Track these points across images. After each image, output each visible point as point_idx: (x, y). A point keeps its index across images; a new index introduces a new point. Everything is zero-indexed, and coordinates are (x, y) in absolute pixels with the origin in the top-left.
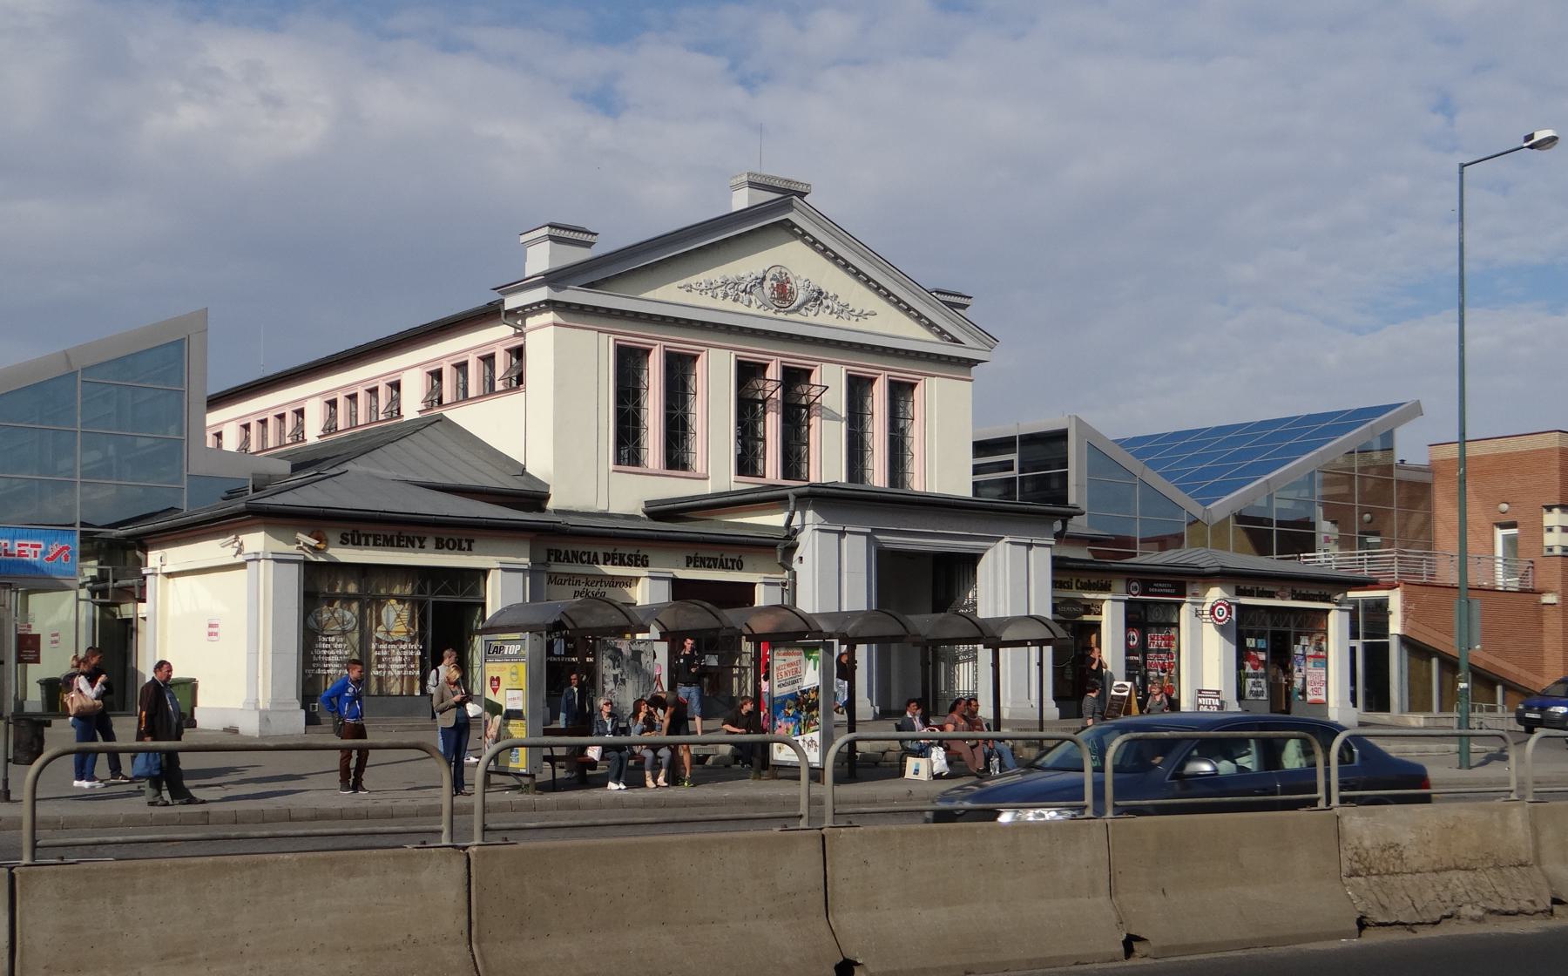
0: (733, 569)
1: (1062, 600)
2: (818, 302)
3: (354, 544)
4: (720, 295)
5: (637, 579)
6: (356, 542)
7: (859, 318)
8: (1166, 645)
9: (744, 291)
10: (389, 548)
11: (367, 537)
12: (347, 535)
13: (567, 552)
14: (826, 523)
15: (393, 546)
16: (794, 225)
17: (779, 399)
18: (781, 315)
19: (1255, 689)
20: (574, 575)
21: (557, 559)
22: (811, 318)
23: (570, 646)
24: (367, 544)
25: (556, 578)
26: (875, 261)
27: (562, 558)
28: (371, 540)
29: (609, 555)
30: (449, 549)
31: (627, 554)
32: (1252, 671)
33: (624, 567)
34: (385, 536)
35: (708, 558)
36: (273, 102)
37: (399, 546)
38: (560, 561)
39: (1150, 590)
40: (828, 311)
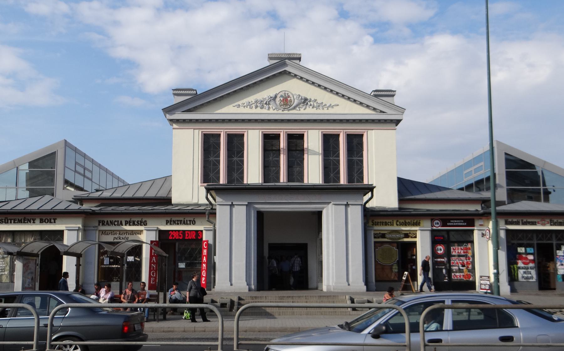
0: (190, 224)
1: (389, 231)
2: (305, 104)
3: (5, 223)
4: (254, 107)
5: (141, 231)
6: (6, 222)
7: (329, 108)
8: (464, 253)
9: (266, 104)
10: (20, 224)
11: (11, 220)
12: (3, 220)
13: (107, 221)
14: (224, 201)
15: (22, 223)
16: (290, 73)
17: (285, 148)
18: (286, 112)
19: (525, 275)
20: (114, 231)
21: (103, 224)
23: (111, 260)
24: (11, 223)
25: (105, 233)
26: (332, 82)
27: (105, 224)
28: (13, 221)
29: (127, 221)
30: (46, 223)
32: (523, 265)
33: (135, 226)
34: (18, 219)
36: (531, 66)
37: (24, 222)
38: (104, 225)
39: (448, 224)
40: (311, 107)
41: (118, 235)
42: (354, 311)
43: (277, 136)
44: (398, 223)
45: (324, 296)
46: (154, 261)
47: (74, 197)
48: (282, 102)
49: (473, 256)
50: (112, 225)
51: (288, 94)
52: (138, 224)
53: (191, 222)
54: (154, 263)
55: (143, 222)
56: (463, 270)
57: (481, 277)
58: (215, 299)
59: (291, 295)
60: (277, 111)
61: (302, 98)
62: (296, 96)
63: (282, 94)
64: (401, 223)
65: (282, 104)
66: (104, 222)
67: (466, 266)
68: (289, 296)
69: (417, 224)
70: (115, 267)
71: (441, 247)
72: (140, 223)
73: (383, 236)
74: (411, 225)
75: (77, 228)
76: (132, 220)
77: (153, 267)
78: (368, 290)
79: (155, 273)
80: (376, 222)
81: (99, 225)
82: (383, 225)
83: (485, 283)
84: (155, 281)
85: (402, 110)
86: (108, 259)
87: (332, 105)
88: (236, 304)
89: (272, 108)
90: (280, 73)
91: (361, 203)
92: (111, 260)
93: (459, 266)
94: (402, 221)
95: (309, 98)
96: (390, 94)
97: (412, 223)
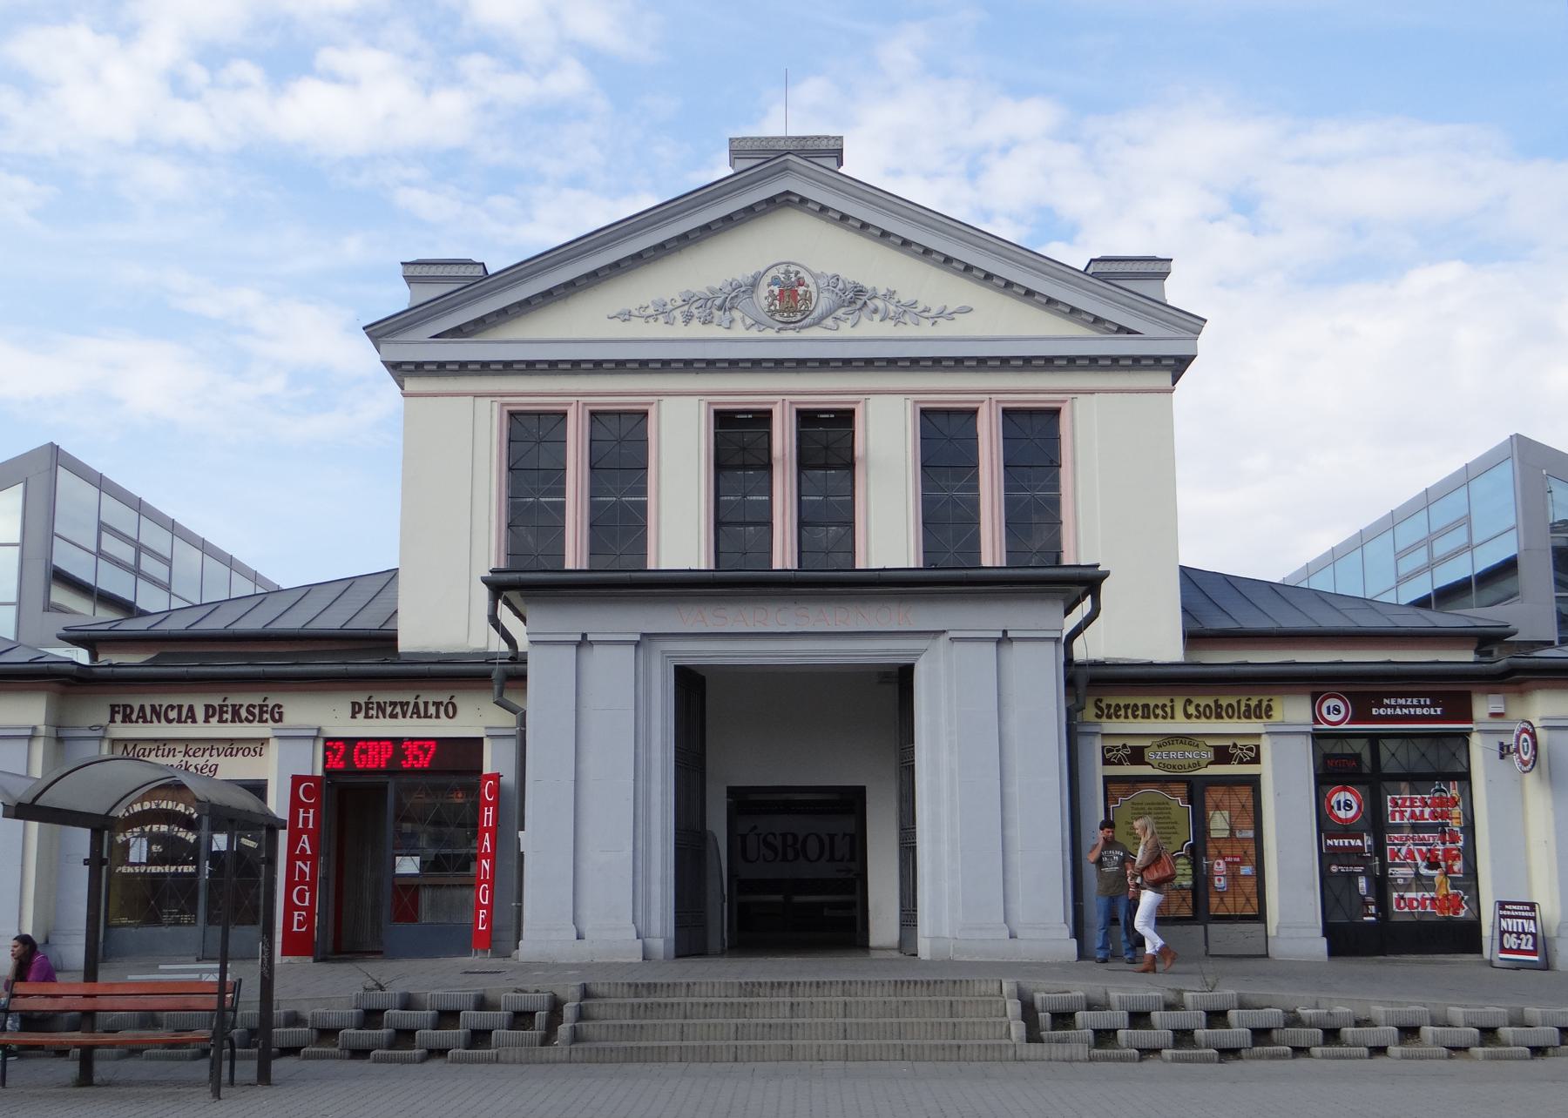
0: (438, 716)
4: (680, 318)
5: (264, 741)
8: (1434, 815)
9: (720, 308)
13: (142, 708)
18: (790, 334)
20: (165, 741)
21: (127, 719)
22: (846, 330)
25: (134, 748)
29: (360, 705)
31: (1132, 704)
35: (391, 703)
38: (131, 721)
39: (1375, 711)
41: (179, 756)
42: (1032, 1045)
43: (763, 418)
44: (1191, 710)
45: (916, 983)
46: (303, 849)
47: (64, 632)
48: (777, 302)
49: (1470, 828)
50: (159, 722)
51: (797, 273)
52: (251, 718)
53: (442, 709)
54: (303, 857)
55: (269, 709)
56: (1432, 878)
57: (1502, 905)
58: (490, 996)
59: (789, 979)
60: (760, 331)
61: (845, 284)
62: (825, 280)
63: (779, 272)
64: (1201, 709)
65: (778, 308)
66: (128, 710)
67: (1443, 864)
68: (779, 984)
69: (1261, 712)
70: (167, 870)
71: (1349, 796)
72: (259, 714)
73: (1137, 756)
74: (1239, 718)
75: (29, 732)
76: (229, 702)
77: (302, 872)
78: (1082, 954)
79: (307, 894)
80: (1109, 706)
81: (112, 721)
82: (1135, 717)
83: (1520, 930)
84: (309, 920)
85: (1194, 324)
86: (145, 843)
87: (947, 312)
88: (569, 1011)
89: (743, 321)
90: (771, 201)
91: (1057, 635)
92: (154, 848)
93: (1416, 865)
94: (1203, 701)
95: (868, 285)
96: (1155, 269)
97: (1243, 708)
